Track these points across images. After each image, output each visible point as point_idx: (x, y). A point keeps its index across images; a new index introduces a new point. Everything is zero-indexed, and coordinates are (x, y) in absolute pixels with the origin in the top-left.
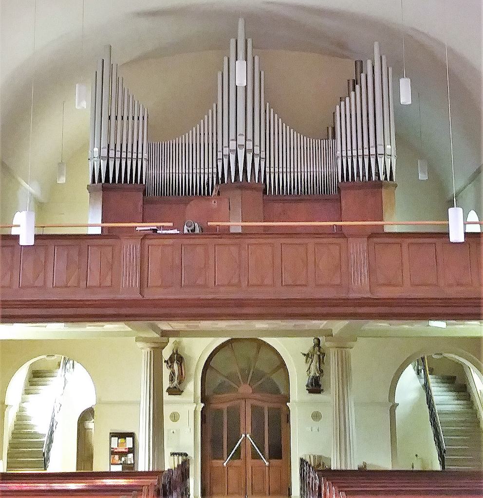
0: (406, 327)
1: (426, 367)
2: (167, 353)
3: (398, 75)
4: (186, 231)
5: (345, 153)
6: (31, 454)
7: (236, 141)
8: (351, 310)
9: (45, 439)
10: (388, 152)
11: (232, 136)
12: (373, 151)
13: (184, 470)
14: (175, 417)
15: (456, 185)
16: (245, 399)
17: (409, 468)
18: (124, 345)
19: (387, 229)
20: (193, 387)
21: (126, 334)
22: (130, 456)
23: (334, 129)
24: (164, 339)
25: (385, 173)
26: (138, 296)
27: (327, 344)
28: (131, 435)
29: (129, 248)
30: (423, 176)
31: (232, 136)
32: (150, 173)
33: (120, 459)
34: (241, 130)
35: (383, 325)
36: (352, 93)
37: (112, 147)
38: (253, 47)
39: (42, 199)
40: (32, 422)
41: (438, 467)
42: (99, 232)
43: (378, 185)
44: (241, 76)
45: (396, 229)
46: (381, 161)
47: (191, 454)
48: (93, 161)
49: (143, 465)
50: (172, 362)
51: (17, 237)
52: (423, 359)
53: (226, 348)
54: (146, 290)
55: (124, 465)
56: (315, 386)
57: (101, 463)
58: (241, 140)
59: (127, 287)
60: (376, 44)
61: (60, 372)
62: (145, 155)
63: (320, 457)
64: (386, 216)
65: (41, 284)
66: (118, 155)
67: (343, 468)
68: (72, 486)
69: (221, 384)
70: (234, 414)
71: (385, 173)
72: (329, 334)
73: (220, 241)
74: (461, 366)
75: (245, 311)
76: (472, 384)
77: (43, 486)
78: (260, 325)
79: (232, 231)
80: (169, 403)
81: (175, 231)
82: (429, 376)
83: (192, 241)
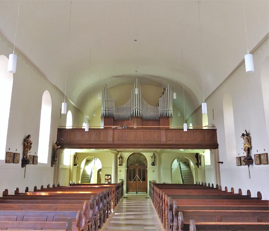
0: (174, 150)
1: (180, 160)
2: (119, 156)
3: (173, 92)
4: (123, 128)
5: (161, 110)
6: (87, 180)
7: (136, 107)
8: (161, 146)
9: (90, 176)
10: (171, 110)
11: (135, 105)
12: (167, 109)
13: (122, 184)
14: (120, 171)
15: (187, 117)
16: (137, 167)
17: (175, 183)
18: (109, 154)
19: (170, 128)
20: (125, 164)
21: (109, 152)
22: (110, 180)
23: (158, 104)
24: (118, 153)
25: (170, 114)
26: (112, 143)
27: (156, 154)
28: (110, 175)
29: (111, 132)
30: (179, 115)
31: (135, 105)
32: (115, 114)
33: (107, 181)
34: (137, 104)
35: (169, 150)
36: (163, 96)
37: (106, 108)
38: (140, 84)
39: (90, 120)
40: (87, 172)
41: (182, 183)
42: (103, 128)
43: (168, 117)
44: (137, 92)
45: (172, 128)
46: (169, 112)
47: (124, 180)
48: (102, 111)
49: (113, 182)
50: (120, 158)
51: (84, 129)
52: (179, 158)
53: (133, 155)
54: (114, 141)
55: (108, 182)
56: (153, 164)
57: (103, 181)
58: (137, 106)
59: (110, 140)
60: (168, 85)
61: (93, 160)
62: (114, 110)
63: (154, 181)
64: (170, 124)
65: (90, 140)
66: (108, 110)
67: (159, 183)
68: (96, 186)
69: (131, 163)
70: (134, 170)
71: (170, 114)
72: (156, 152)
73: (131, 130)
74: (188, 160)
75: (137, 146)
76: (190, 164)
77: (89, 186)
78: (141, 150)
79: (134, 128)
80: (119, 168)
81: (121, 128)
82: (180, 162)
83: (125, 130)
